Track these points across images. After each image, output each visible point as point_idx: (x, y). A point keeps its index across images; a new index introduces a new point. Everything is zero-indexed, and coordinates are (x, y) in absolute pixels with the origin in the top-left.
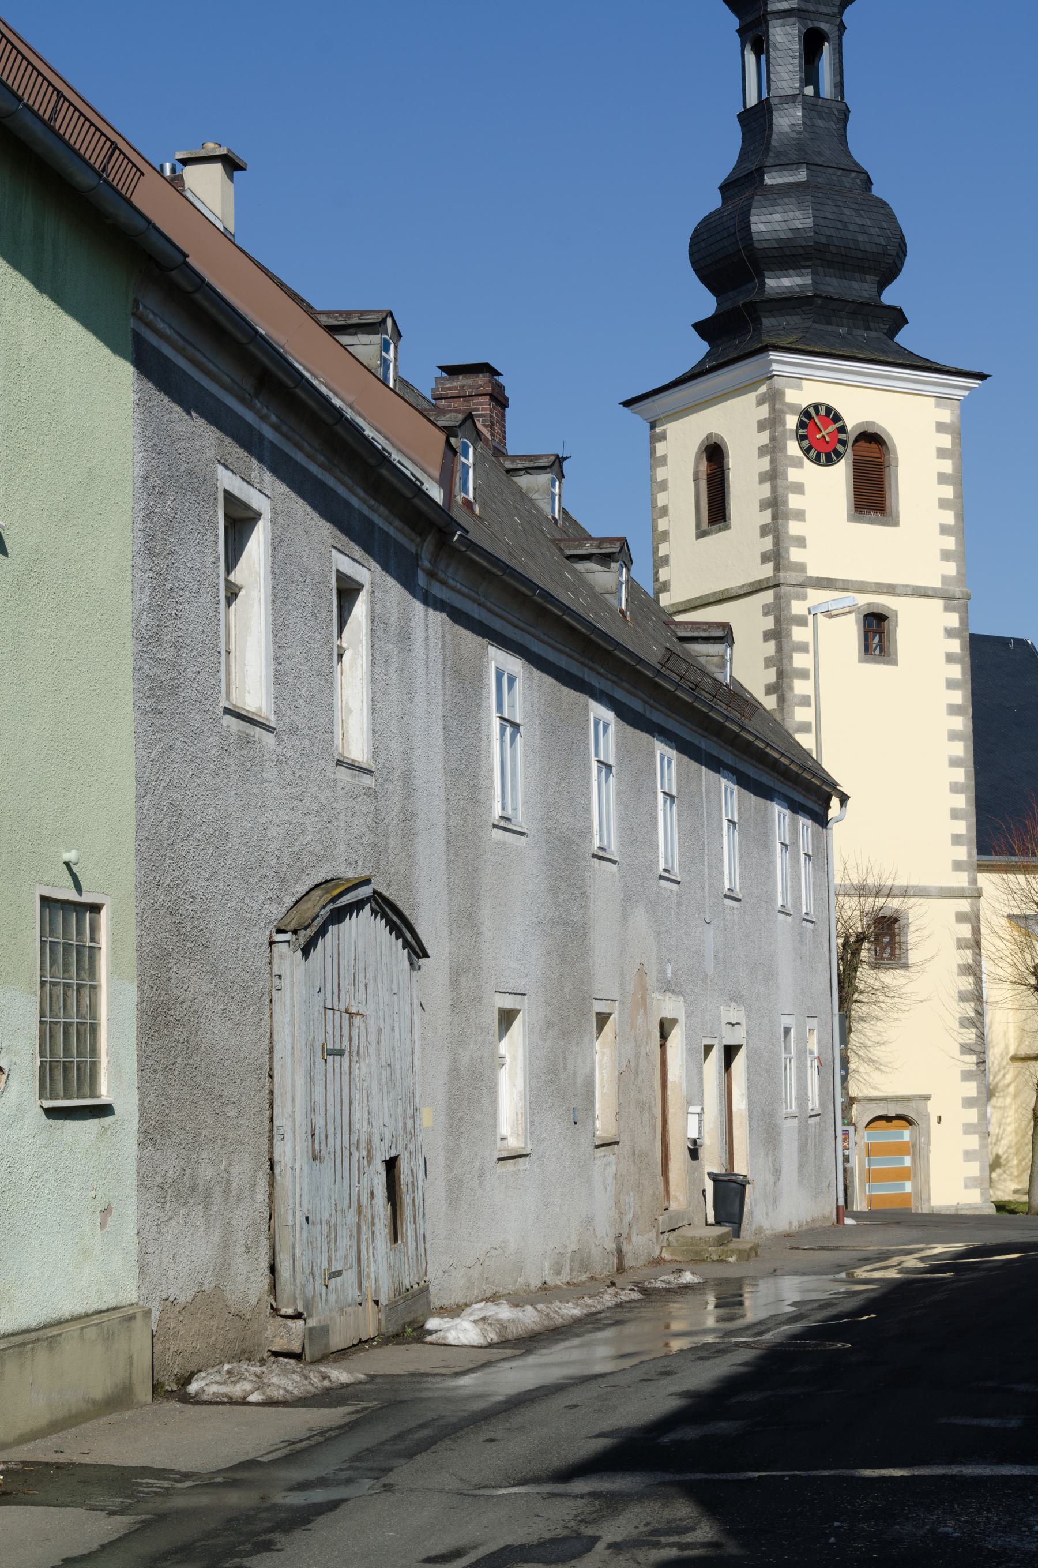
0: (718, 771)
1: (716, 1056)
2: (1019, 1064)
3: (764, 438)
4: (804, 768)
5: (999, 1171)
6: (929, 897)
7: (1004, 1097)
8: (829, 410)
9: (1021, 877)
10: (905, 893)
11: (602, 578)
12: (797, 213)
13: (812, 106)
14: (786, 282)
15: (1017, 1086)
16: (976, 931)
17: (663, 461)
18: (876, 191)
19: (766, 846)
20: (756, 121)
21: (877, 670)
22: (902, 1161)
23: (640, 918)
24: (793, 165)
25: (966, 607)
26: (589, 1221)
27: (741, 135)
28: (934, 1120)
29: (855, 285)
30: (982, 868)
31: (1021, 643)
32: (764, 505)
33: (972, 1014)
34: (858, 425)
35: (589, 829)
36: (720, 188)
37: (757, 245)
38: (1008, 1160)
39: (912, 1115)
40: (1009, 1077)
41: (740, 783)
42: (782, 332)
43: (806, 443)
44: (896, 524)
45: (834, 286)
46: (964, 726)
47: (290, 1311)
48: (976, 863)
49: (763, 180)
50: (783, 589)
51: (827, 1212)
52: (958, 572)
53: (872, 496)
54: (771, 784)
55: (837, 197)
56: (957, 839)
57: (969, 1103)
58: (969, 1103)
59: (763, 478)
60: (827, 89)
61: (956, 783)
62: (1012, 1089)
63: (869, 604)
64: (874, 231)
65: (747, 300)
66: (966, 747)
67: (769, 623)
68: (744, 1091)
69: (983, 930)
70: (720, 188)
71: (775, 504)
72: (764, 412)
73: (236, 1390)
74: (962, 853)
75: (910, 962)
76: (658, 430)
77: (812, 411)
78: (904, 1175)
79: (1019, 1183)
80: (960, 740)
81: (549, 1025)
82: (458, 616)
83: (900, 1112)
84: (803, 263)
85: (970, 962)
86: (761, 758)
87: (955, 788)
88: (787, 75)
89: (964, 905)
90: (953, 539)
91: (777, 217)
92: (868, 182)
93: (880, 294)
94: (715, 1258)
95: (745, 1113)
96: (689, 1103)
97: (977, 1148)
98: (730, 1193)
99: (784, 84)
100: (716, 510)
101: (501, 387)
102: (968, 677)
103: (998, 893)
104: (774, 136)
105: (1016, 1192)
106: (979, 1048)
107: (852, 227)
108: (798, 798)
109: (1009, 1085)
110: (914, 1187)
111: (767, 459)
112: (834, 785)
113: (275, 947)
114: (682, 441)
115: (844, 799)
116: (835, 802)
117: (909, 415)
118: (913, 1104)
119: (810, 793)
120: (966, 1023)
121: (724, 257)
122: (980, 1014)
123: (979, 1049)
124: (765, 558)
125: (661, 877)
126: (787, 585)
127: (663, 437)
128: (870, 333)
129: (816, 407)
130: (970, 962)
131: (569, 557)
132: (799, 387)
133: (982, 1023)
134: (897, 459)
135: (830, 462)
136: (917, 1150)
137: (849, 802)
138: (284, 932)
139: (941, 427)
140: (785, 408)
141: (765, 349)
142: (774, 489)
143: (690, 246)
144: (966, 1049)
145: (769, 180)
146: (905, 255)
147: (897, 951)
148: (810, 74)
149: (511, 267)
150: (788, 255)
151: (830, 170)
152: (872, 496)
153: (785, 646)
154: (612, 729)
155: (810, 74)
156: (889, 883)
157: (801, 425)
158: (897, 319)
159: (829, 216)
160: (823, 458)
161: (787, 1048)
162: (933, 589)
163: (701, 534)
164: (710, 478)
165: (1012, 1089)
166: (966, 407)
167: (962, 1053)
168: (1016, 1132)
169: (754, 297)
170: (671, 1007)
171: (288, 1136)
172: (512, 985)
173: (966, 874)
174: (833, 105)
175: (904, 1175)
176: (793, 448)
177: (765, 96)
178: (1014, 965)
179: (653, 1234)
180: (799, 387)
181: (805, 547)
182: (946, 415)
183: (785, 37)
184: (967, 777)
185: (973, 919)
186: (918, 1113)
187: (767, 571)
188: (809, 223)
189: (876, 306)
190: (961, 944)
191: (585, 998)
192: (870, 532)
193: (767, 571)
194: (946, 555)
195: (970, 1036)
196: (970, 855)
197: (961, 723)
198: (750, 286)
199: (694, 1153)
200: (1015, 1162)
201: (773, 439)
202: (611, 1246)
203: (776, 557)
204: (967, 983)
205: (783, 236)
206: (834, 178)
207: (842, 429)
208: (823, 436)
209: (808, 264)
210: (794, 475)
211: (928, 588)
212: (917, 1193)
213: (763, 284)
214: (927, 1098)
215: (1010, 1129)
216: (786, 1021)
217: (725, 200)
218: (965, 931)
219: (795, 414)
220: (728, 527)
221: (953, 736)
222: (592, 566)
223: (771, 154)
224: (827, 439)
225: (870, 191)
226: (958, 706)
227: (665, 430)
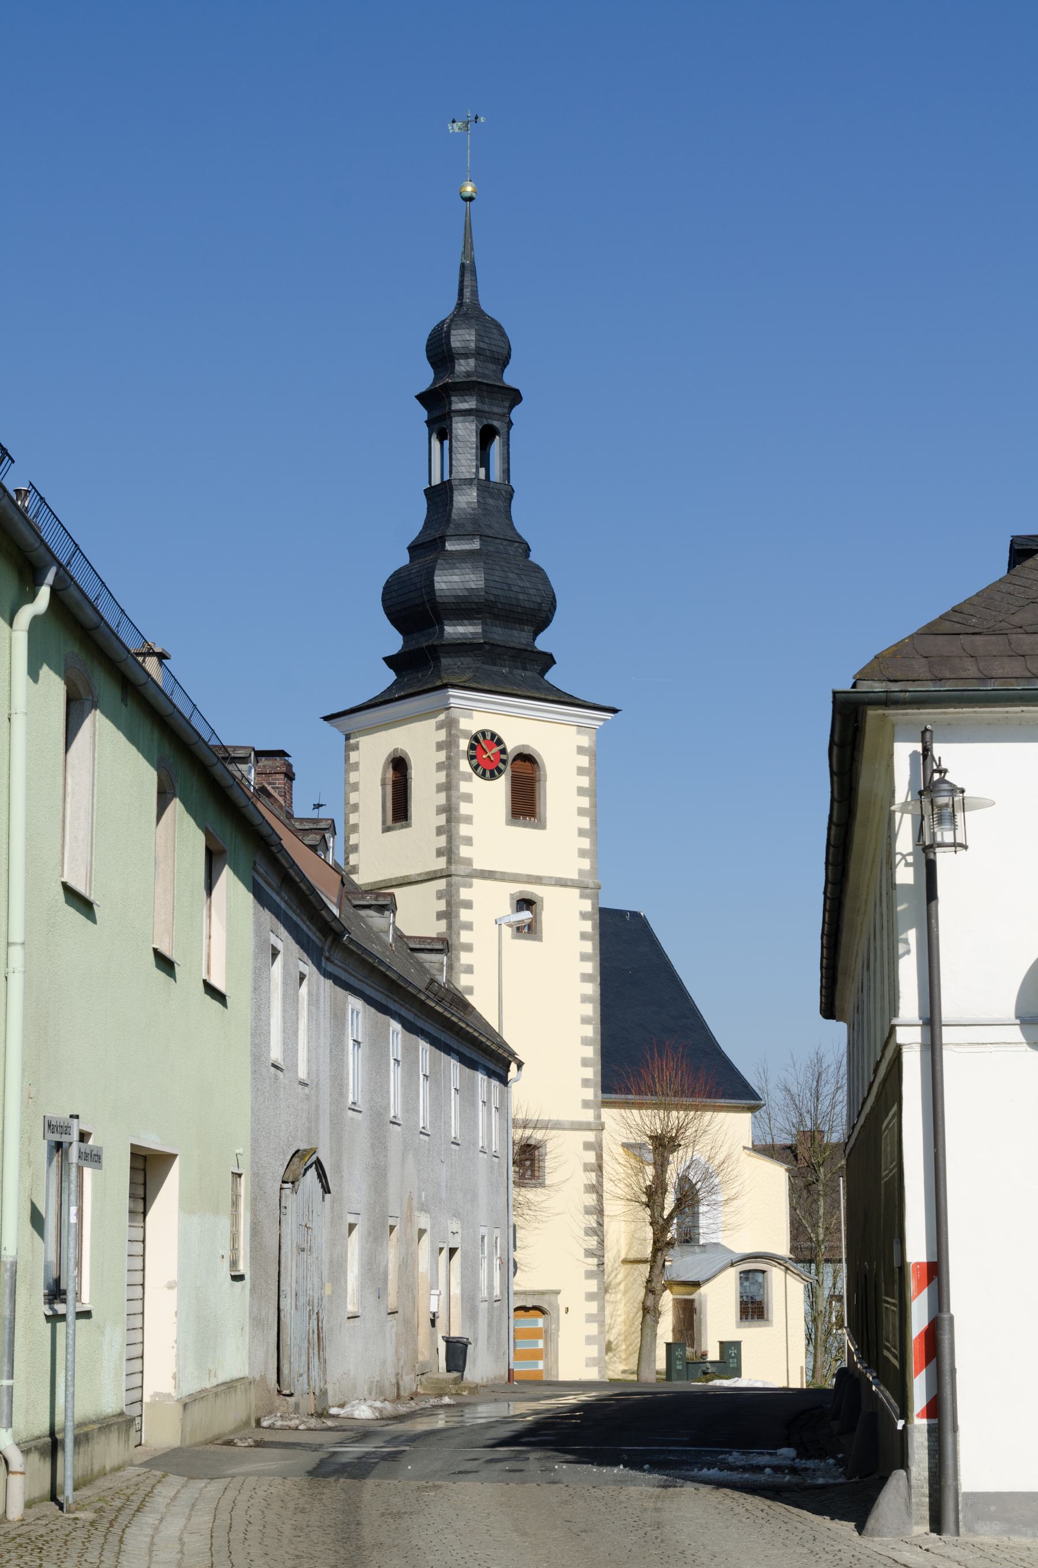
0: (449, 1055)
1: (445, 1253)
2: (628, 1266)
3: (442, 756)
4: (500, 1046)
5: (610, 1354)
6: (564, 1129)
7: (616, 1293)
8: (493, 735)
9: (635, 1112)
10: (546, 1126)
11: (376, 920)
12: (472, 576)
13: (485, 487)
14: (461, 629)
15: (627, 1285)
16: (600, 1157)
17: (356, 767)
18: (533, 557)
19: (474, 1105)
20: (439, 496)
22: (537, 1344)
23: (410, 1160)
24: (470, 536)
25: (597, 895)
26: (384, 1363)
27: (426, 506)
28: (562, 1311)
29: (515, 633)
30: (605, 1104)
31: (635, 915)
32: (440, 810)
33: (595, 1225)
34: (516, 748)
35: (389, 1104)
36: (409, 548)
37: (439, 600)
38: (617, 1345)
39: (545, 1306)
40: (620, 1277)
41: (432, 1044)
42: (457, 671)
43: (475, 762)
44: (544, 827)
45: (500, 635)
47: (288, 1392)
48: (600, 1099)
49: (444, 546)
50: (454, 879)
51: (502, 1374)
52: (591, 867)
53: (525, 805)
54: (476, 1059)
55: (503, 564)
56: (586, 1083)
57: (590, 1297)
58: (590, 1297)
59: (440, 788)
60: (496, 475)
62: (622, 1287)
64: (532, 592)
65: (430, 643)
67: (442, 905)
68: (459, 1281)
69: (606, 1157)
70: (409, 548)
71: (449, 810)
72: (442, 735)
73: (293, 1423)
74: (590, 1094)
75: (547, 1182)
76: (352, 741)
78: (537, 1355)
79: (626, 1365)
81: (369, 1233)
82: (338, 981)
83: (536, 1304)
85: (594, 1182)
86: (473, 1042)
87: (585, 1041)
88: (466, 464)
89: (590, 1136)
91: (456, 578)
92: (527, 550)
93: (534, 640)
94: (454, 1392)
95: (459, 1297)
96: (432, 1288)
97: (596, 1333)
98: (457, 1352)
99: (463, 469)
100: (400, 810)
101: (290, 766)
102: (598, 952)
103: (617, 1127)
104: (454, 511)
105: (624, 1372)
106: (598, 1253)
107: (514, 588)
108: (492, 1066)
109: (620, 1283)
110: (546, 1365)
111: (443, 773)
112: (512, 1054)
113: (283, 1192)
114: (373, 750)
115: (520, 1065)
116: (513, 1067)
117: (553, 738)
118: (546, 1297)
119: (487, 1056)
120: (590, 1232)
121: (410, 603)
122: (601, 1224)
123: (599, 1253)
124: (440, 853)
125: (421, 1133)
127: (356, 747)
128: (524, 672)
129: (483, 733)
130: (594, 1182)
131: (355, 906)
132: (471, 717)
133: (602, 1232)
135: (493, 777)
136: (548, 1335)
137: (524, 1067)
138: (287, 1182)
139: (581, 750)
141: (445, 686)
142: (449, 798)
143: (383, 594)
144: (589, 1253)
145: (449, 546)
147: (537, 1174)
148: (484, 461)
149: (277, 653)
150: (464, 608)
151: (498, 541)
152: (525, 805)
153: (454, 924)
154: (400, 1036)
155: (484, 461)
156: (535, 1118)
157: (472, 747)
158: (547, 661)
159: (497, 579)
161: (483, 1252)
162: (572, 880)
163: (386, 829)
164: (395, 784)
165: (622, 1287)
166: (600, 736)
167: (586, 1256)
168: (625, 1323)
169: (436, 643)
170: (423, 1221)
171: (288, 1296)
172: (356, 1209)
173: (592, 1111)
174: (502, 487)
175: (537, 1355)
176: (465, 766)
177: (446, 478)
178: (629, 1186)
179: (412, 1376)
180: (471, 717)
181: (471, 845)
182: (585, 741)
183: (465, 431)
184: (595, 1032)
185: (597, 1148)
186: (550, 1304)
187: (441, 863)
188: (481, 584)
189: (532, 651)
190: (587, 1168)
191: (385, 1216)
192: (523, 834)
193: (441, 863)
194: (582, 853)
195: (593, 1242)
196: (596, 1096)
197: (591, 989)
198: (431, 630)
199: (433, 1323)
200: (624, 1347)
201: (449, 758)
202: (394, 1381)
203: (448, 852)
204: (591, 1199)
205: (460, 594)
207: (504, 751)
210: (464, 787)
212: (548, 1369)
213: (442, 630)
214: (558, 1292)
215: (620, 1319)
216: (483, 1231)
217: (412, 559)
218: (591, 1157)
220: (409, 826)
221: (585, 999)
222: (371, 912)
223: (451, 525)
225: (529, 556)
226: (589, 975)
227: (358, 742)
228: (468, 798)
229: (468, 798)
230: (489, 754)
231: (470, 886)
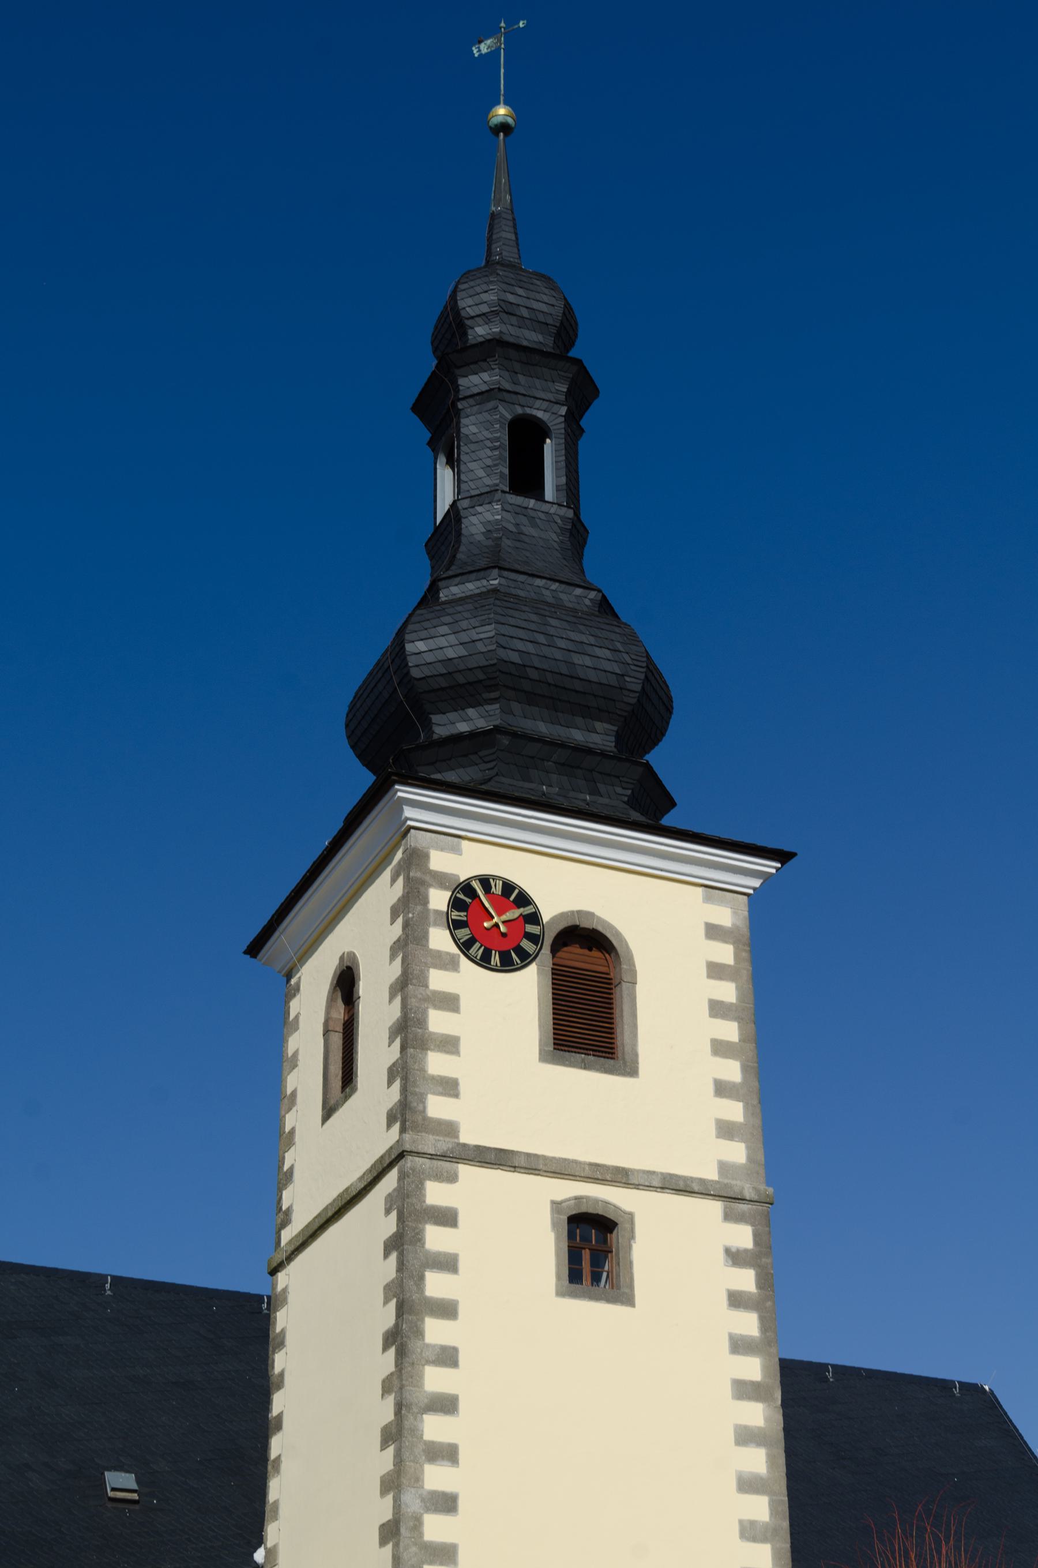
8: (508, 887)
21: (590, 1312)
31: (972, 1390)
43: (464, 934)
46: (766, 1420)
52: (749, 1158)
61: (753, 1523)
63: (578, 1199)
66: (771, 1460)
71: (409, 1031)
77: (476, 885)
80: (759, 1444)
84: (486, 696)
90: (741, 1105)
104: (462, 548)
126: (419, 1154)
129: (485, 881)
132: (457, 851)
134: (633, 973)
135: (507, 965)
140: (427, 878)
146: (671, 713)
157: (455, 904)
160: (496, 959)
162: (702, 1181)
176: (440, 939)
180: (457, 851)
181: (457, 1096)
182: (725, 915)
192: (581, 1083)
203: (405, 1114)
206: (547, 593)
207: (534, 918)
208: (496, 925)
209: (493, 695)
210: (438, 980)
211: (692, 1179)
219: (446, 888)
224: (503, 929)
228: (450, 1002)
229: (450, 1002)
230: (496, 920)
231: (452, 1178)
